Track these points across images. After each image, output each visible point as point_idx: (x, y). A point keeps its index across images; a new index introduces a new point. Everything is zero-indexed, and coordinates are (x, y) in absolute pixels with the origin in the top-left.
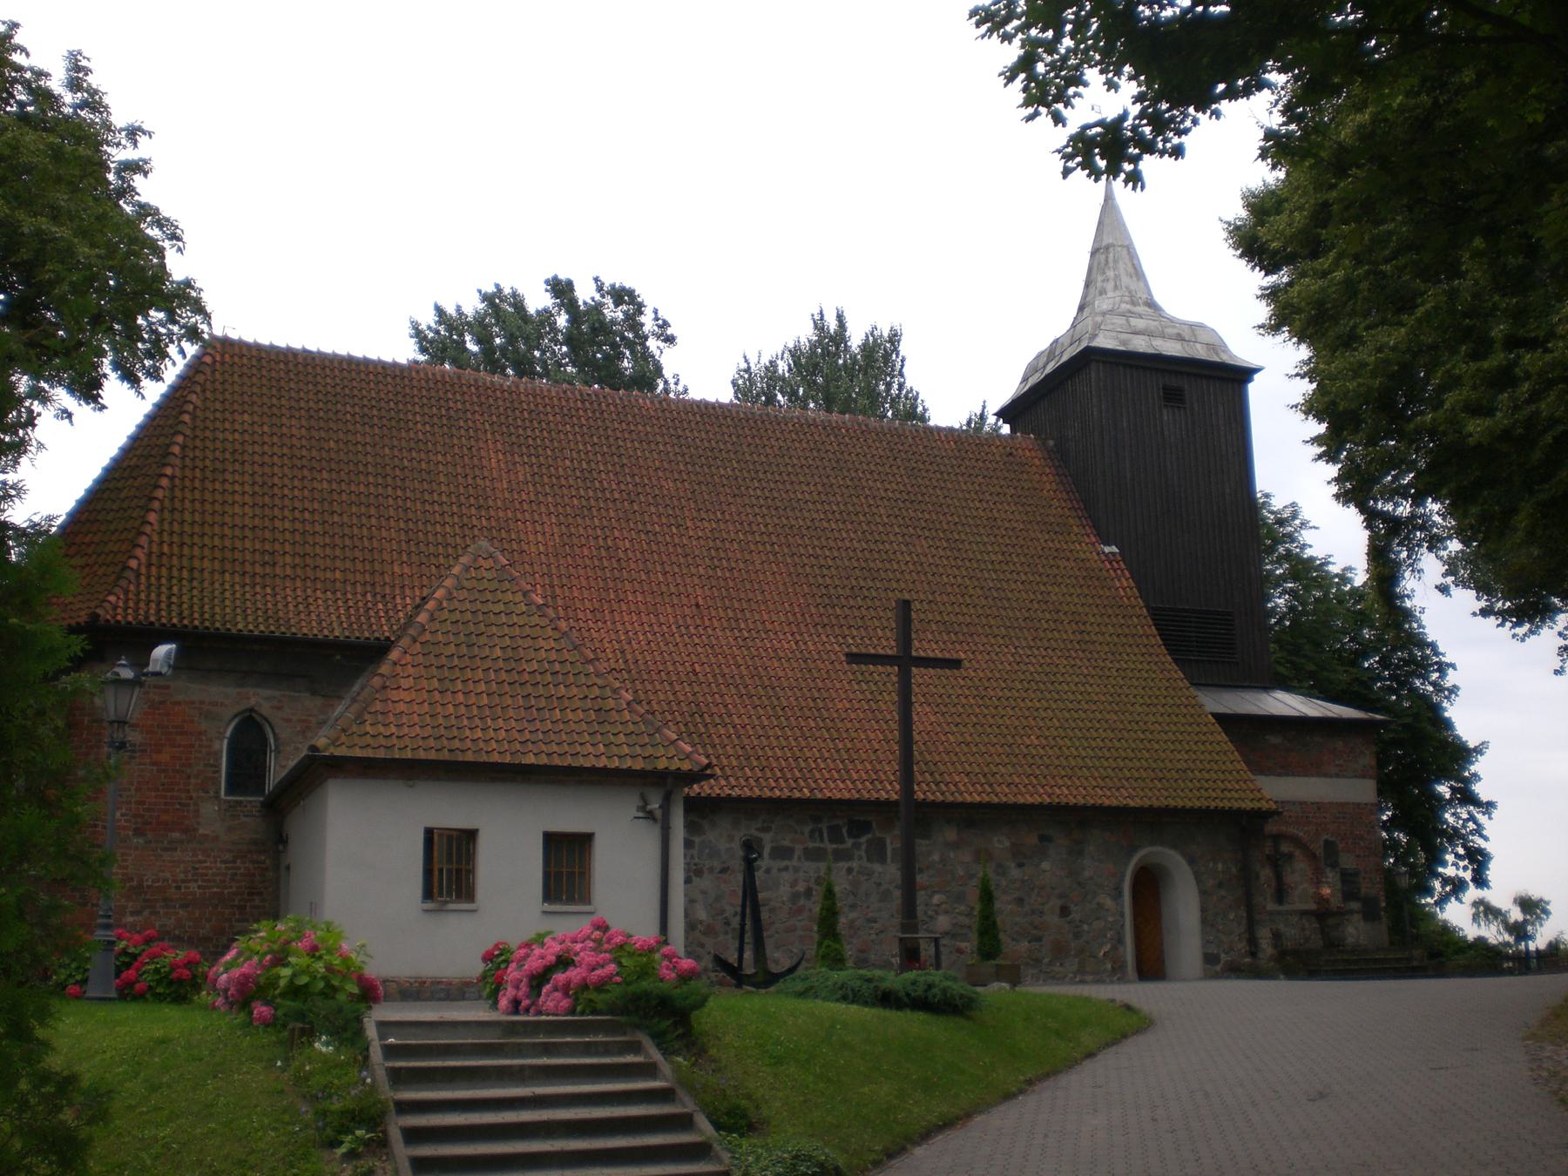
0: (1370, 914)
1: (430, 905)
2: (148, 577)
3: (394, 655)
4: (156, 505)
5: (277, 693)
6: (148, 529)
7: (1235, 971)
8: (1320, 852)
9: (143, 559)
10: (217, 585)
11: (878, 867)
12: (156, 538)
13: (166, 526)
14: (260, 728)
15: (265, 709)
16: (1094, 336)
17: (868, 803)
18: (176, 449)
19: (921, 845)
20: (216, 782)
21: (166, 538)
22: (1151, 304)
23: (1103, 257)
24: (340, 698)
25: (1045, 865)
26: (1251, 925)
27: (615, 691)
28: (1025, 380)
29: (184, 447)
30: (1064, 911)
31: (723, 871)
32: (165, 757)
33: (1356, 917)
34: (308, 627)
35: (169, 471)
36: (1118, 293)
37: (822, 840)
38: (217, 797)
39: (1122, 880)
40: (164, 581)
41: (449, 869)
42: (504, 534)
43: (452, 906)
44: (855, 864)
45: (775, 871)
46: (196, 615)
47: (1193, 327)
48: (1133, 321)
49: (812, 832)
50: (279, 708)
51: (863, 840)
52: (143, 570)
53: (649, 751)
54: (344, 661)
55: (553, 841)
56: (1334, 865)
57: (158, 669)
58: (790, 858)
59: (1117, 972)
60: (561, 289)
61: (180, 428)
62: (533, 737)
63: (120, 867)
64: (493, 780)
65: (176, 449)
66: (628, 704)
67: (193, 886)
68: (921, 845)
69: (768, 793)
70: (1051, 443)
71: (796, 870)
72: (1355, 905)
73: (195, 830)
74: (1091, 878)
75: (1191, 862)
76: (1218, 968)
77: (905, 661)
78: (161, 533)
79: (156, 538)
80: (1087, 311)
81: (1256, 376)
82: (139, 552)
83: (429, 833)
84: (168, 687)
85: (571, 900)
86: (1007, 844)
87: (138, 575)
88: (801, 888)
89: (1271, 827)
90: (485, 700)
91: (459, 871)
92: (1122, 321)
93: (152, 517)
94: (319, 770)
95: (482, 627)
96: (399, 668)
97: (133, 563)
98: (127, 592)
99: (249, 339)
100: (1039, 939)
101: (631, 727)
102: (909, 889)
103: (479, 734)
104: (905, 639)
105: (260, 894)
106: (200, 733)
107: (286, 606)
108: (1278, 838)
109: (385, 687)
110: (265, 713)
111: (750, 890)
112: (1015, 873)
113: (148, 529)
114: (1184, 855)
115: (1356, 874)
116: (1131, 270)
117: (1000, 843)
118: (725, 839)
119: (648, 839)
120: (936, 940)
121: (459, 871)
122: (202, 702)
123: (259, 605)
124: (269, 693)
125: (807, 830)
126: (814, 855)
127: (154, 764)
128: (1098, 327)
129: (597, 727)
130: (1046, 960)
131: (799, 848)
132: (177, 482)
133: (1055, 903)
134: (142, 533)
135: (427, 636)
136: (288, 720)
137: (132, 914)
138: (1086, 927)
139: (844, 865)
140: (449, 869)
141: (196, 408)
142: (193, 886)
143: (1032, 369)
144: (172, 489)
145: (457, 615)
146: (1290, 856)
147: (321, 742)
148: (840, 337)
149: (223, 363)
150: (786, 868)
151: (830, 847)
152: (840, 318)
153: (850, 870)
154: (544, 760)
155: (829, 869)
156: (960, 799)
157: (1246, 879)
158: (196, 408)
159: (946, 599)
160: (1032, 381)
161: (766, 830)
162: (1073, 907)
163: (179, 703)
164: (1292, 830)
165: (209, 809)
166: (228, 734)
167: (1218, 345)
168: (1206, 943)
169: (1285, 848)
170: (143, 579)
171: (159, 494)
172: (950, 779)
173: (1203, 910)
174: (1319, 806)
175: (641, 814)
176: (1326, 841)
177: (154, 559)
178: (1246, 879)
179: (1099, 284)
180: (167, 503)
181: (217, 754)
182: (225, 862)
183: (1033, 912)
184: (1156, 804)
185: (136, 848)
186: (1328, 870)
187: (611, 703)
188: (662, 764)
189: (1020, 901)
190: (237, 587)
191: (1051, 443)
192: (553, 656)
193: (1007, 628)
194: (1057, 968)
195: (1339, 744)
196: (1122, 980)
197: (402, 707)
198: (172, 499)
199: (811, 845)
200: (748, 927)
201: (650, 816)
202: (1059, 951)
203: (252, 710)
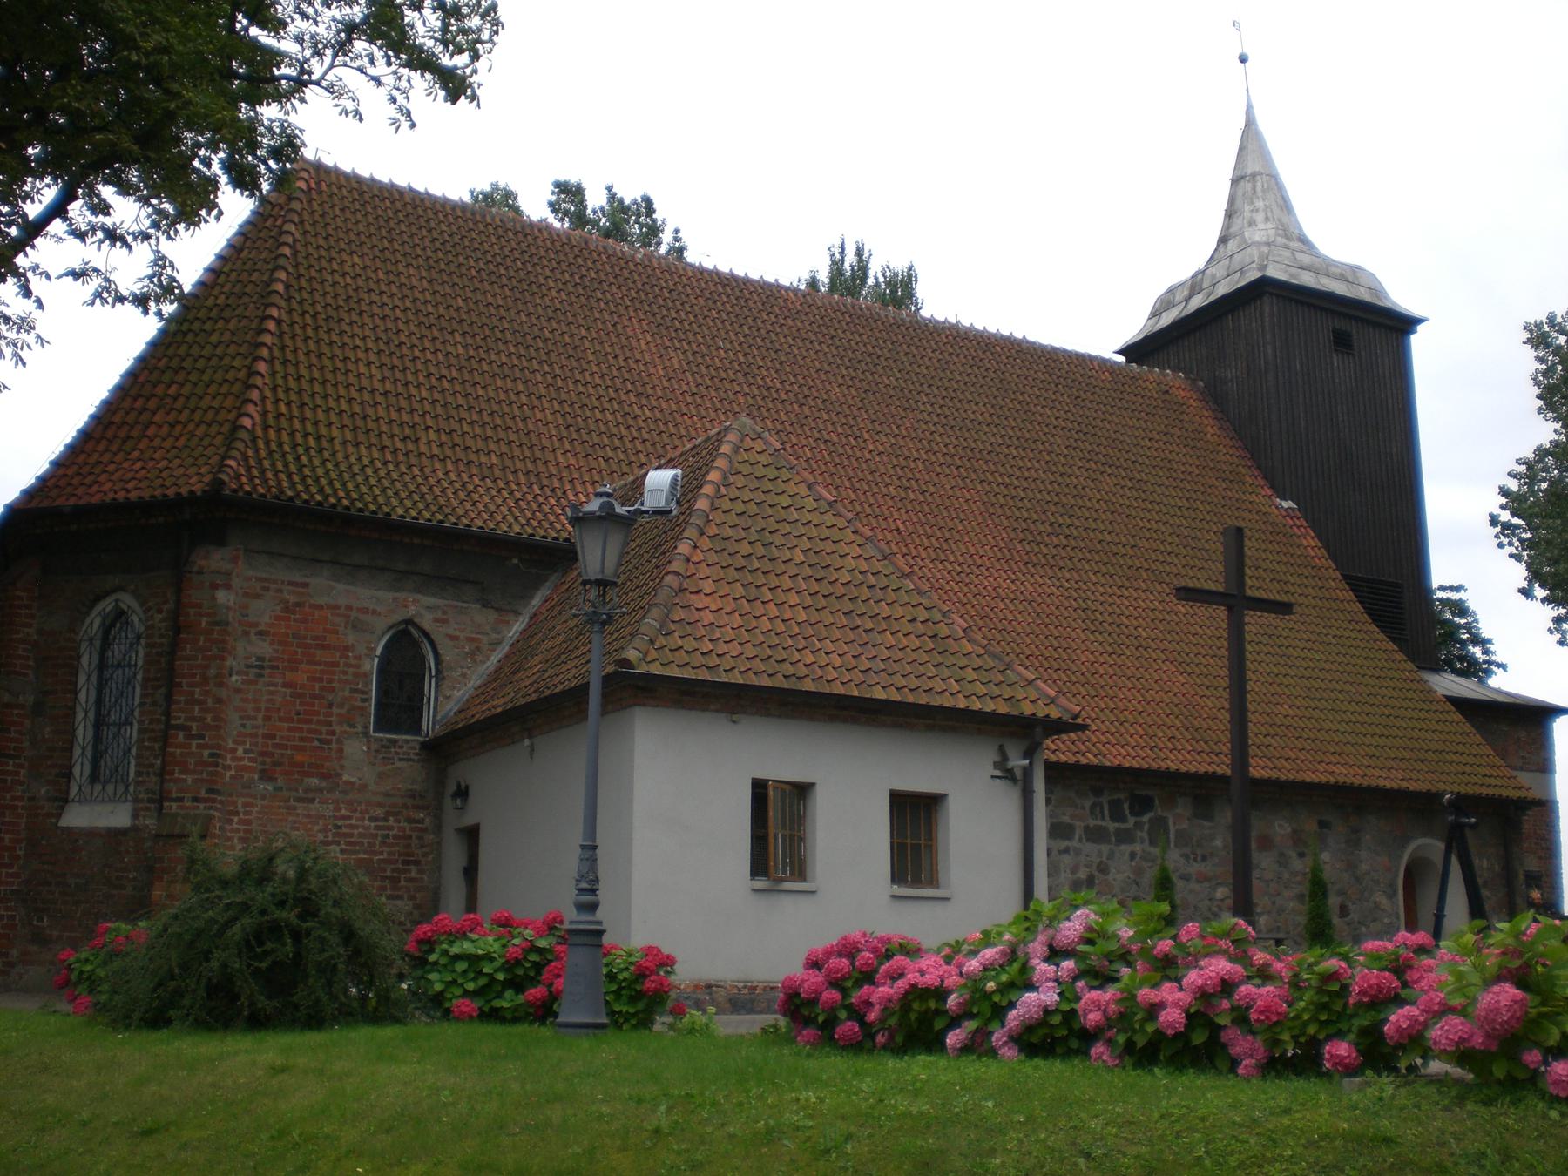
1: (761, 883)
2: (267, 443)
5: (440, 602)
6: (259, 381)
9: (258, 419)
14: (416, 644)
15: (427, 622)
18: (280, 288)
20: (363, 711)
22: (1303, 240)
23: (1249, 186)
24: (517, 613)
28: (1155, 314)
29: (288, 287)
32: (301, 678)
35: (275, 312)
36: (1269, 225)
37: (1103, 818)
38: (366, 734)
43: (788, 886)
44: (1137, 848)
47: (1355, 269)
49: (1093, 806)
50: (444, 621)
51: (1145, 818)
57: (661, 503)
60: (569, 193)
63: (241, 822)
64: (832, 719)
68: (1257, 826)
71: (1078, 852)
73: (340, 775)
80: (1232, 245)
81: (1420, 328)
83: (760, 789)
84: (306, 585)
87: (254, 439)
90: (802, 616)
91: (916, 848)
97: (247, 422)
99: (346, 167)
105: (417, 863)
106: (347, 648)
109: (682, 590)
110: (426, 625)
116: (1280, 201)
119: (1006, 803)
122: (350, 608)
124: (431, 601)
125: (1088, 804)
126: (1095, 835)
127: (285, 685)
131: (1079, 825)
136: (453, 638)
139: (1126, 848)
140: (777, 832)
141: (295, 241)
147: (632, 654)
148: (862, 269)
149: (320, 193)
150: (1066, 851)
151: (1112, 826)
152: (859, 252)
153: (1133, 855)
154: (895, 696)
155: (1111, 856)
158: (295, 241)
160: (1167, 319)
162: (1351, 907)
163: (320, 607)
165: (356, 749)
166: (378, 652)
167: (1377, 290)
170: (261, 443)
175: (998, 773)
179: (1247, 214)
181: (367, 676)
182: (372, 819)
188: (1027, 709)
191: (1201, 384)
195: (1523, 734)
197: (708, 617)
198: (283, 348)
199: (1092, 823)
201: (1009, 775)
203: (409, 622)
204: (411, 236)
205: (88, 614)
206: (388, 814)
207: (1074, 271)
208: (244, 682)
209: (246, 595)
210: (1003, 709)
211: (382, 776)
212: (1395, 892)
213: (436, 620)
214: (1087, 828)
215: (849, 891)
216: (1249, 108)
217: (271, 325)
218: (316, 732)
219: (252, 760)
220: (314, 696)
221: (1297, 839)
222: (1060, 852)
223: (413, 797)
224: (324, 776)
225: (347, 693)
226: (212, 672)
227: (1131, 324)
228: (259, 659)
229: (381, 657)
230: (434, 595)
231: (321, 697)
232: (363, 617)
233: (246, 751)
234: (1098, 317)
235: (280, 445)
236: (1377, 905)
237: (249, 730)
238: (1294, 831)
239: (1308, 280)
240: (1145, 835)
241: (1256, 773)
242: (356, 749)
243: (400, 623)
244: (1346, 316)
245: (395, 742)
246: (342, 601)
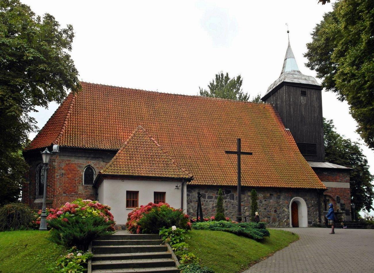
0: (347, 214)
2: (65, 136)
3: (119, 152)
4: (67, 119)
7: (316, 226)
8: (336, 199)
10: (81, 137)
11: (232, 201)
12: (67, 127)
13: (69, 124)
15: (92, 165)
16: (285, 79)
17: (230, 186)
18: (71, 107)
19: (242, 196)
20: (82, 182)
21: (69, 127)
25: (271, 201)
26: (320, 215)
27: (171, 160)
28: (268, 91)
30: (275, 211)
32: (70, 176)
33: (344, 214)
34: (102, 147)
35: (70, 112)
38: (82, 185)
39: (289, 204)
40: (69, 136)
42: (147, 126)
44: (227, 200)
45: (208, 202)
46: (76, 144)
48: (294, 76)
50: (96, 165)
51: (229, 195)
52: (64, 134)
53: (178, 173)
54: (108, 154)
55: (129, 193)
58: (212, 199)
59: (288, 225)
61: (72, 102)
62: (151, 170)
65: (71, 107)
66: (174, 162)
68: (242, 196)
69: (207, 184)
70: (274, 105)
72: (344, 212)
74: (282, 204)
75: (306, 200)
76: (311, 225)
77: (239, 153)
78: (68, 126)
79: (67, 127)
82: (63, 130)
84: (70, 160)
86: (262, 196)
87: (63, 136)
89: (324, 194)
92: (292, 75)
93: (66, 122)
94: (102, 177)
95: (140, 145)
96: (120, 154)
97: (62, 133)
98: (60, 139)
100: (270, 217)
101: (174, 168)
102: (240, 206)
103: (139, 169)
107: (97, 142)
108: (326, 196)
110: (92, 166)
111: (199, 205)
112: (264, 202)
113: (65, 125)
114: (304, 199)
115: (344, 204)
118: (195, 194)
120: (245, 217)
121: (133, 201)
123: (91, 142)
124: (93, 162)
125: (216, 192)
127: (67, 177)
128: (285, 77)
129: (166, 168)
130: (271, 222)
131: (214, 196)
132: (72, 114)
133: (273, 209)
134: (63, 126)
135: (127, 147)
138: (280, 215)
141: (76, 98)
144: (71, 116)
145: (134, 143)
146: (328, 200)
147: (102, 171)
150: (211, 201)
154: (154, 175)
156: (251, 185)
157: (319, 204)
159: (249, 141)
161: (207, 192)
162: (277, 210)
163: (73, 164)
164: (329, 194)
165: (81, 188)
166: (84, 171)
168: (309, 219)
169: (327, 198)
170: (64, 136)
171: (67, 117)
172: (248, 181)
173: (308, 211)
174: (336, 189)
176: (337, 197)
177: (67, 132)
178: (319, 204)
180: (69, 119)
181: (82, 175)
183: (268, 211)
184: (298, 187)
185: (64, 196)
186: (337, 203)
187: (169, 163)
188: (181, 176)
189: (265, 209)
190: (86, 138)
192: (156, 152)
193: (263, 147)
194: (273, 224)
195: (341, 175)
196: (289, 227)
200: (199, 213)
202: (274, 221)
203: (89, 165)
204: (110, 93)
205: (36, 167)
208: (60, 177)
209: (59, 163)
210: (176, 176)
212: (289, 208)
213: (94, 165)
214: (216, 197)
216: (289, 43)
217: (69, 114)
218: (73, 185)
219: (62, 190)
220: (72, 179)
221: (264, 197)
222: (210, 201)
223: (91, 195)
224: (75, 193)
225: (78, 178)
226: (53, 176)
228: (62, 173)
230: (94, 160)
231: (74, 179)
232: (80, 165)
233: (61, 189)
235: (68, 136)
236: (284, 210)
237: (61, 185)
238: (264, 196)
240: (229, 197)
241: (242, 185)
242: (81, 188)
243: (88, 165)
244: (304, 88)
245: (88, 186)
246: (77, 163)
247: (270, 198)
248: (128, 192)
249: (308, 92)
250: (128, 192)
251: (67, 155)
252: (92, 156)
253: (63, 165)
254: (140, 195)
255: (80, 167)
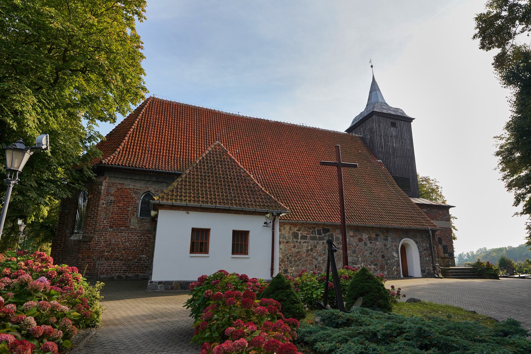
25: (378, 243)
28: (353, 123)
30: (383, 257)
31: (287, 242)
32: (121, 205)
41: (200, 242)
51: (327, 234)
56: (441, 244)
67: (127, 244)
71: (308, 243)
85: (241, 253)
88: (309, 248)
104: (339, 171)
105: (148, 246)
114: (414, 241)
117: (365, 236)
126: (313, 238)
137: (107, 252)
140: (200, 242)
142: (127, 244)
143: (355, 120)
150: (305, 242)
155: (318, 243)
160: (356, 122)
166: (142, 198)
168: (421, 267)
203: (149, 191)
206: (142, 235)
207: (336, 113)
211: (140, 226)
215: (220, 258)
221: (370, 239)
227: (348, 125)
229: (142, 200)
234: (341, 124)
239: (385, 111)
247: (376, 239)
248: (235, 232)
249: (398, 123)
250: (235, 232)
251: (121, 177)
252: (154, 179)
253: (113, 190)
254: (251, 236)
255: (136, 193)
